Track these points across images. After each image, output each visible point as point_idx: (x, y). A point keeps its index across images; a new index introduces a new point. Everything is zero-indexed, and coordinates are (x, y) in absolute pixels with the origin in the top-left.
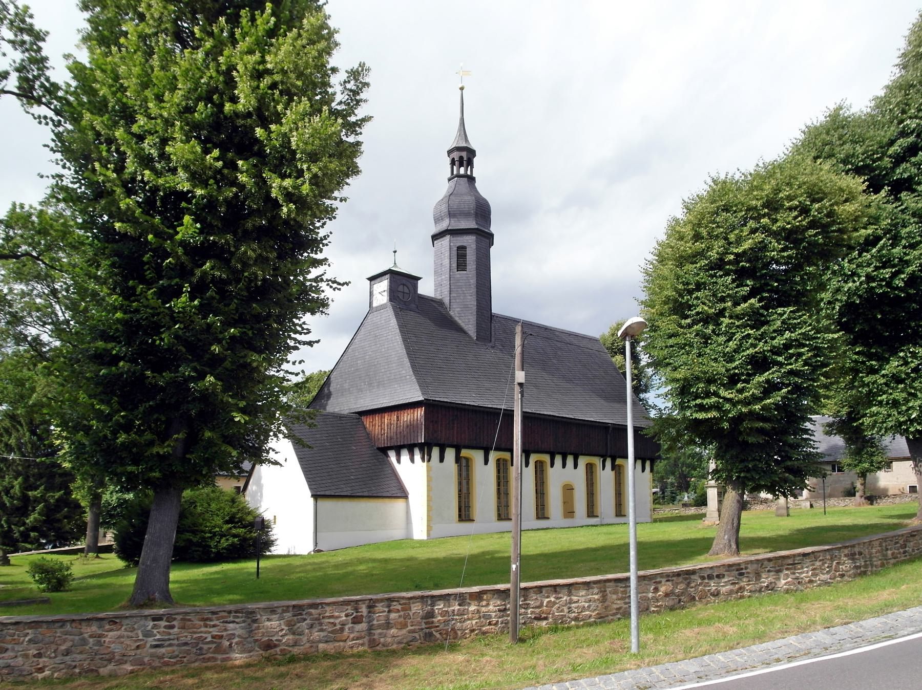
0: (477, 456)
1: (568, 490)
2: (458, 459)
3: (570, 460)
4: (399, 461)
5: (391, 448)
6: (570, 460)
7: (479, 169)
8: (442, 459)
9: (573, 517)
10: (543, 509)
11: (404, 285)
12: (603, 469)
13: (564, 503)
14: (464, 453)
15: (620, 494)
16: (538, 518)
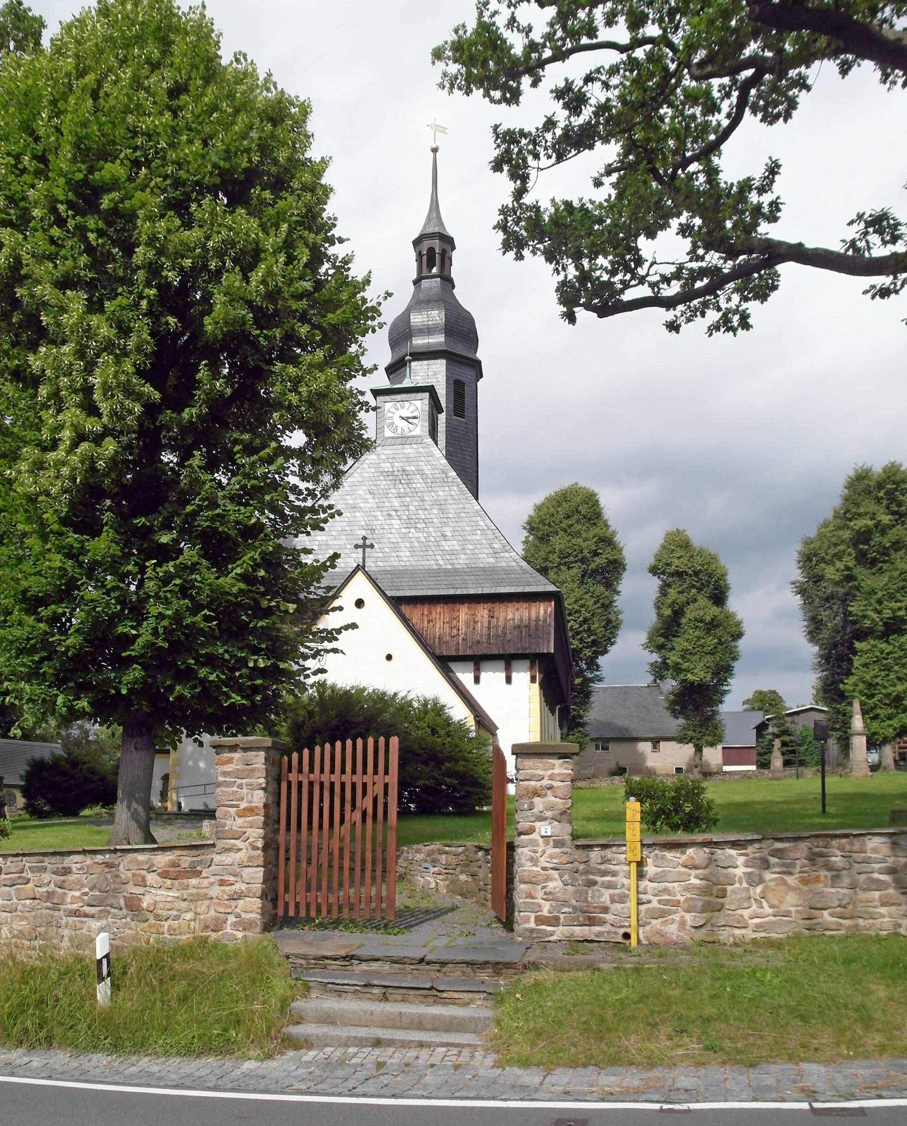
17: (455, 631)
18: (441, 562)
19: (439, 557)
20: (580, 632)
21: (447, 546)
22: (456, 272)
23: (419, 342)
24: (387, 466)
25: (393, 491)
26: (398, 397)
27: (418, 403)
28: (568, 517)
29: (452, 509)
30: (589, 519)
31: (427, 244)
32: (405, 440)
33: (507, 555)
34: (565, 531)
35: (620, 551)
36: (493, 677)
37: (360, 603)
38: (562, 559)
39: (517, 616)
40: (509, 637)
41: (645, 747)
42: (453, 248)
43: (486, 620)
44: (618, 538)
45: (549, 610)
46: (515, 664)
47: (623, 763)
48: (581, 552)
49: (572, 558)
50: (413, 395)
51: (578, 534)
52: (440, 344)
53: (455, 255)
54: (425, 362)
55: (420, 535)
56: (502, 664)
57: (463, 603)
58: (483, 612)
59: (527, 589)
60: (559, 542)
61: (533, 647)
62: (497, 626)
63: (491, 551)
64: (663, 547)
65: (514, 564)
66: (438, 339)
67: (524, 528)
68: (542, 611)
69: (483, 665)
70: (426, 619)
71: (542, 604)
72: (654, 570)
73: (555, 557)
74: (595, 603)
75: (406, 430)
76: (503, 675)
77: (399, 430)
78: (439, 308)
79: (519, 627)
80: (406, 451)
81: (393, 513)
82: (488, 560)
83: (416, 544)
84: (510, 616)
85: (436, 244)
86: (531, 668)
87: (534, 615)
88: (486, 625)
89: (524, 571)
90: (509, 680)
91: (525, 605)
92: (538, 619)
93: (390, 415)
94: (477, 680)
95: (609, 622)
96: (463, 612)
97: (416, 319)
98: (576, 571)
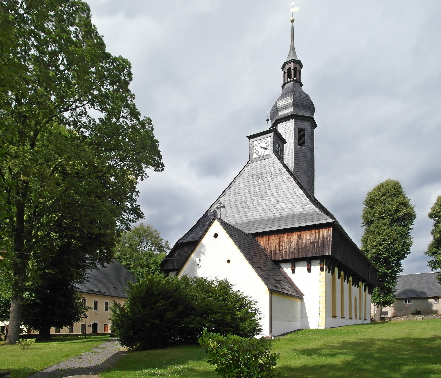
17: (281, 248)
18: (276, 214)
19: (275, 212)
20: (389, 249)
21: (280, 206)
22: (303, 79)
23: (281, 114)
24: (254, 172)
25: (256, 183)
26: (259, 138)
27: (269, 139)
28: (384, 195)
29: (283, 187)
30: (395, 195)
31: (287, 67)
32: (263, 158)
33: (309, 206)
34: (382, 202)
35: (412, 209)
36: (301, 269)
37: (216, 236)
38: (380, 215)
39: (312, 237)
40: (308, 248)
41: (431, 301)
42: (301, 66)
43: (296, 241)
44: (410, 202)
45: (329, 232)
46: (313, 262)
47: (419, 309)
48: (390, 211)
49: (385, 214)
50: (266, 135)
51: (388, 203)
52: (291, 112)
53: (302, 70)
54: (284, 123)
55: (267, 202)
56: (305, 263)
57: (285, 233)
58: (295, 236)
59: (313, 223)
60: (379, 208)
61: (321, 252)
62: (302, 243)
63: (301, 205)
64: (436, 204)
65: (312, 211)
66: (290, 110)
67: (364, 204)
68: (325, 234)
69: (297, 264)
70: (267, 243)
71: (325, 230)
72: (430, 216)
73: (377, 215)
74: (397, 234)
75: (263, 153)
76: (306, 268)
77: (260, 154)
78: (290, 95)
79: (313, 243)
80: (263, 163)
81: (255, 194)
82: (299, 211)
83: (265, 207)
84: (309, 238)
85: (292, 66)
86: (321, 264)
87: (321, 236)
88: (296, 243)
89: (317, 213)
90: (309, 270)
91: (317, 231)
92: (323, 237)
93: (256, 147)
94: (293, 271)
95: (405, 243)
96: (285, 238)
97: (280, 104)
98: (387, 220)
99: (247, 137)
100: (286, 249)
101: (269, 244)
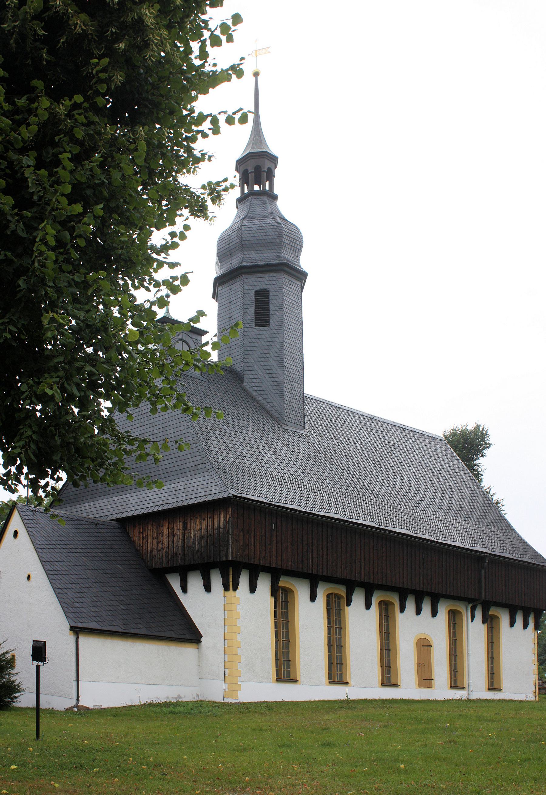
0: (301, 591)
1: (424, 646)
2: (274, 591)
3: (427, 608)
4: (185, 590)
5: (172, 570)
6: (427, 608)
7: (282, 183)
8: (253, 589)
9: (430, 686)
10: (389, 672)
11: (183, 341)
12: (472, 620)
13: (419, 665)
14: (284, 582)
15: (456, 655)
16: (332, 681)
37: (16, 534)
99: (206, 315)
100: (168, 548)
101: (143, 538)
